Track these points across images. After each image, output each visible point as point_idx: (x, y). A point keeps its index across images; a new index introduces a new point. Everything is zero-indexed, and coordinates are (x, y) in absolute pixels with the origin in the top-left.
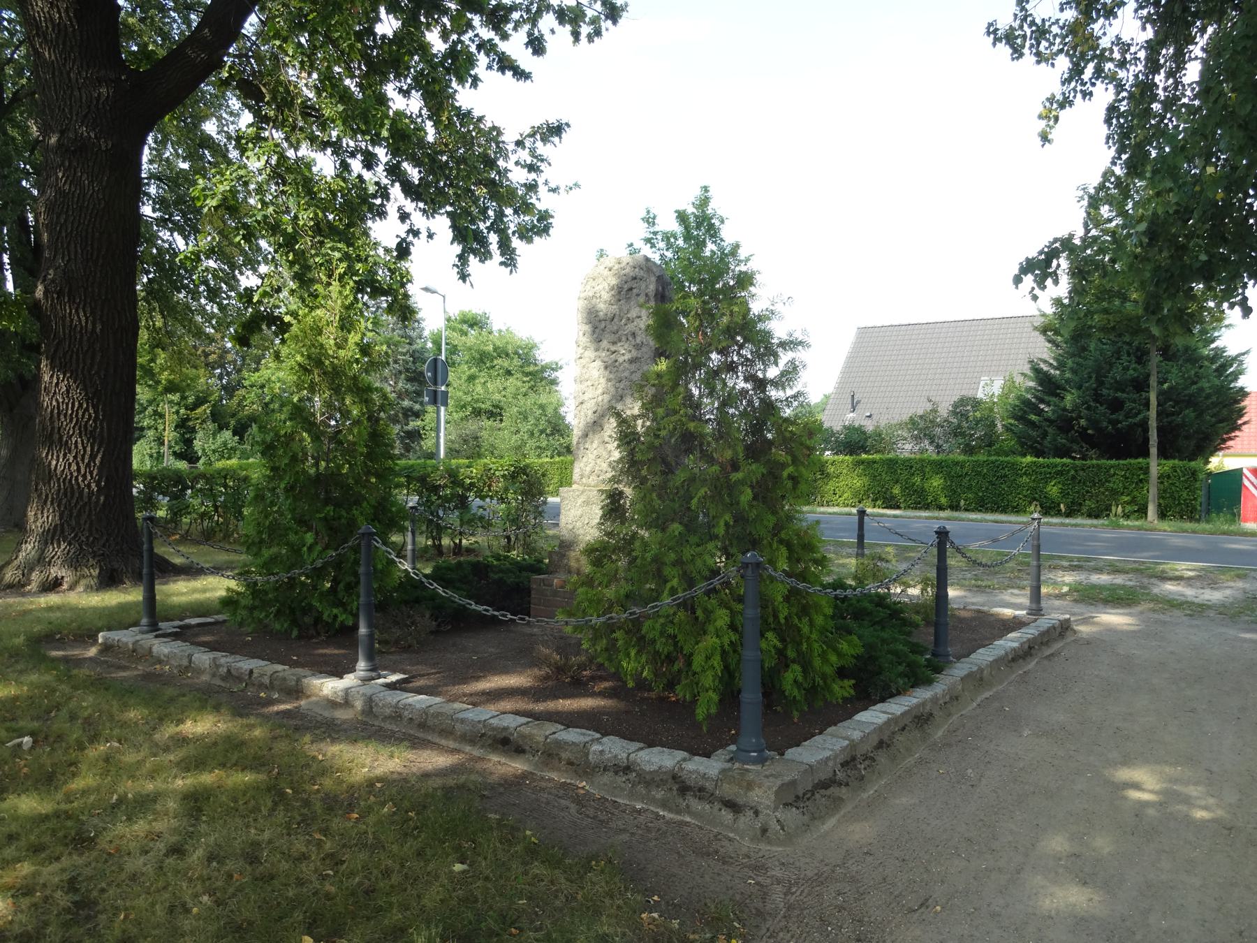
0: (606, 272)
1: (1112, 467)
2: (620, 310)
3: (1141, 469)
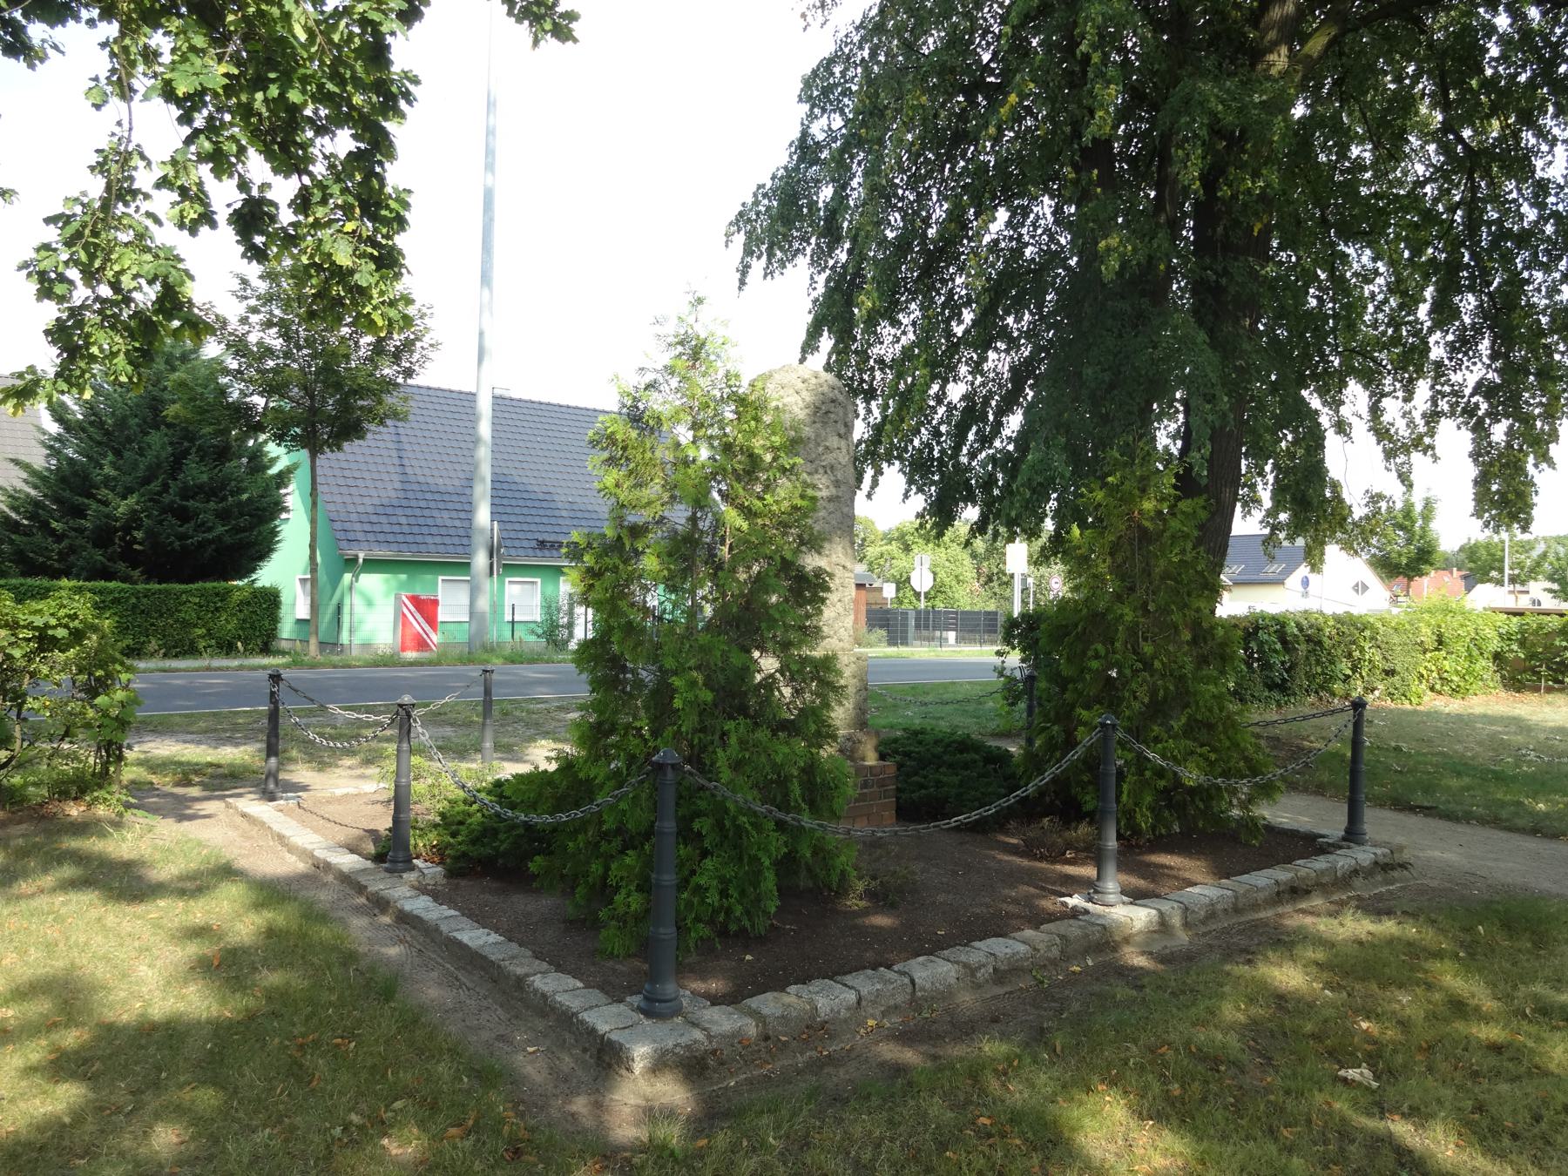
0: (800, 385)
1: (184, 592)
2: (818, 435)
3: (217, 595)
